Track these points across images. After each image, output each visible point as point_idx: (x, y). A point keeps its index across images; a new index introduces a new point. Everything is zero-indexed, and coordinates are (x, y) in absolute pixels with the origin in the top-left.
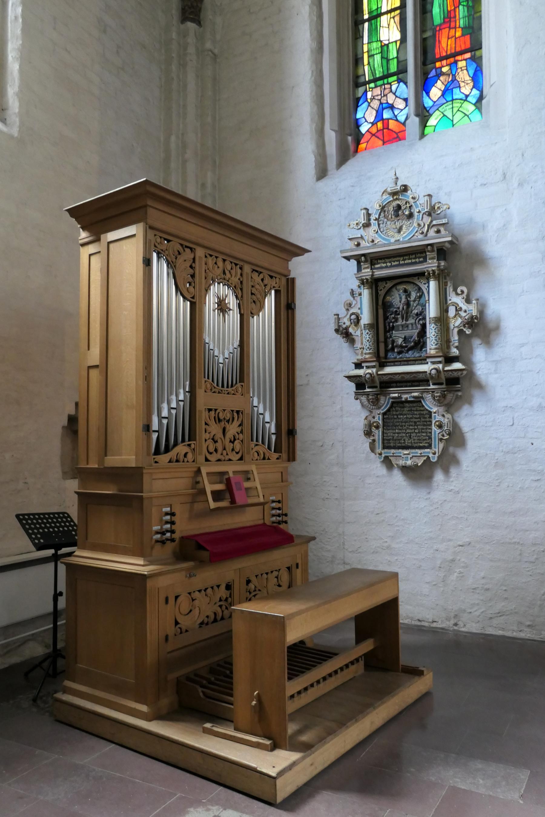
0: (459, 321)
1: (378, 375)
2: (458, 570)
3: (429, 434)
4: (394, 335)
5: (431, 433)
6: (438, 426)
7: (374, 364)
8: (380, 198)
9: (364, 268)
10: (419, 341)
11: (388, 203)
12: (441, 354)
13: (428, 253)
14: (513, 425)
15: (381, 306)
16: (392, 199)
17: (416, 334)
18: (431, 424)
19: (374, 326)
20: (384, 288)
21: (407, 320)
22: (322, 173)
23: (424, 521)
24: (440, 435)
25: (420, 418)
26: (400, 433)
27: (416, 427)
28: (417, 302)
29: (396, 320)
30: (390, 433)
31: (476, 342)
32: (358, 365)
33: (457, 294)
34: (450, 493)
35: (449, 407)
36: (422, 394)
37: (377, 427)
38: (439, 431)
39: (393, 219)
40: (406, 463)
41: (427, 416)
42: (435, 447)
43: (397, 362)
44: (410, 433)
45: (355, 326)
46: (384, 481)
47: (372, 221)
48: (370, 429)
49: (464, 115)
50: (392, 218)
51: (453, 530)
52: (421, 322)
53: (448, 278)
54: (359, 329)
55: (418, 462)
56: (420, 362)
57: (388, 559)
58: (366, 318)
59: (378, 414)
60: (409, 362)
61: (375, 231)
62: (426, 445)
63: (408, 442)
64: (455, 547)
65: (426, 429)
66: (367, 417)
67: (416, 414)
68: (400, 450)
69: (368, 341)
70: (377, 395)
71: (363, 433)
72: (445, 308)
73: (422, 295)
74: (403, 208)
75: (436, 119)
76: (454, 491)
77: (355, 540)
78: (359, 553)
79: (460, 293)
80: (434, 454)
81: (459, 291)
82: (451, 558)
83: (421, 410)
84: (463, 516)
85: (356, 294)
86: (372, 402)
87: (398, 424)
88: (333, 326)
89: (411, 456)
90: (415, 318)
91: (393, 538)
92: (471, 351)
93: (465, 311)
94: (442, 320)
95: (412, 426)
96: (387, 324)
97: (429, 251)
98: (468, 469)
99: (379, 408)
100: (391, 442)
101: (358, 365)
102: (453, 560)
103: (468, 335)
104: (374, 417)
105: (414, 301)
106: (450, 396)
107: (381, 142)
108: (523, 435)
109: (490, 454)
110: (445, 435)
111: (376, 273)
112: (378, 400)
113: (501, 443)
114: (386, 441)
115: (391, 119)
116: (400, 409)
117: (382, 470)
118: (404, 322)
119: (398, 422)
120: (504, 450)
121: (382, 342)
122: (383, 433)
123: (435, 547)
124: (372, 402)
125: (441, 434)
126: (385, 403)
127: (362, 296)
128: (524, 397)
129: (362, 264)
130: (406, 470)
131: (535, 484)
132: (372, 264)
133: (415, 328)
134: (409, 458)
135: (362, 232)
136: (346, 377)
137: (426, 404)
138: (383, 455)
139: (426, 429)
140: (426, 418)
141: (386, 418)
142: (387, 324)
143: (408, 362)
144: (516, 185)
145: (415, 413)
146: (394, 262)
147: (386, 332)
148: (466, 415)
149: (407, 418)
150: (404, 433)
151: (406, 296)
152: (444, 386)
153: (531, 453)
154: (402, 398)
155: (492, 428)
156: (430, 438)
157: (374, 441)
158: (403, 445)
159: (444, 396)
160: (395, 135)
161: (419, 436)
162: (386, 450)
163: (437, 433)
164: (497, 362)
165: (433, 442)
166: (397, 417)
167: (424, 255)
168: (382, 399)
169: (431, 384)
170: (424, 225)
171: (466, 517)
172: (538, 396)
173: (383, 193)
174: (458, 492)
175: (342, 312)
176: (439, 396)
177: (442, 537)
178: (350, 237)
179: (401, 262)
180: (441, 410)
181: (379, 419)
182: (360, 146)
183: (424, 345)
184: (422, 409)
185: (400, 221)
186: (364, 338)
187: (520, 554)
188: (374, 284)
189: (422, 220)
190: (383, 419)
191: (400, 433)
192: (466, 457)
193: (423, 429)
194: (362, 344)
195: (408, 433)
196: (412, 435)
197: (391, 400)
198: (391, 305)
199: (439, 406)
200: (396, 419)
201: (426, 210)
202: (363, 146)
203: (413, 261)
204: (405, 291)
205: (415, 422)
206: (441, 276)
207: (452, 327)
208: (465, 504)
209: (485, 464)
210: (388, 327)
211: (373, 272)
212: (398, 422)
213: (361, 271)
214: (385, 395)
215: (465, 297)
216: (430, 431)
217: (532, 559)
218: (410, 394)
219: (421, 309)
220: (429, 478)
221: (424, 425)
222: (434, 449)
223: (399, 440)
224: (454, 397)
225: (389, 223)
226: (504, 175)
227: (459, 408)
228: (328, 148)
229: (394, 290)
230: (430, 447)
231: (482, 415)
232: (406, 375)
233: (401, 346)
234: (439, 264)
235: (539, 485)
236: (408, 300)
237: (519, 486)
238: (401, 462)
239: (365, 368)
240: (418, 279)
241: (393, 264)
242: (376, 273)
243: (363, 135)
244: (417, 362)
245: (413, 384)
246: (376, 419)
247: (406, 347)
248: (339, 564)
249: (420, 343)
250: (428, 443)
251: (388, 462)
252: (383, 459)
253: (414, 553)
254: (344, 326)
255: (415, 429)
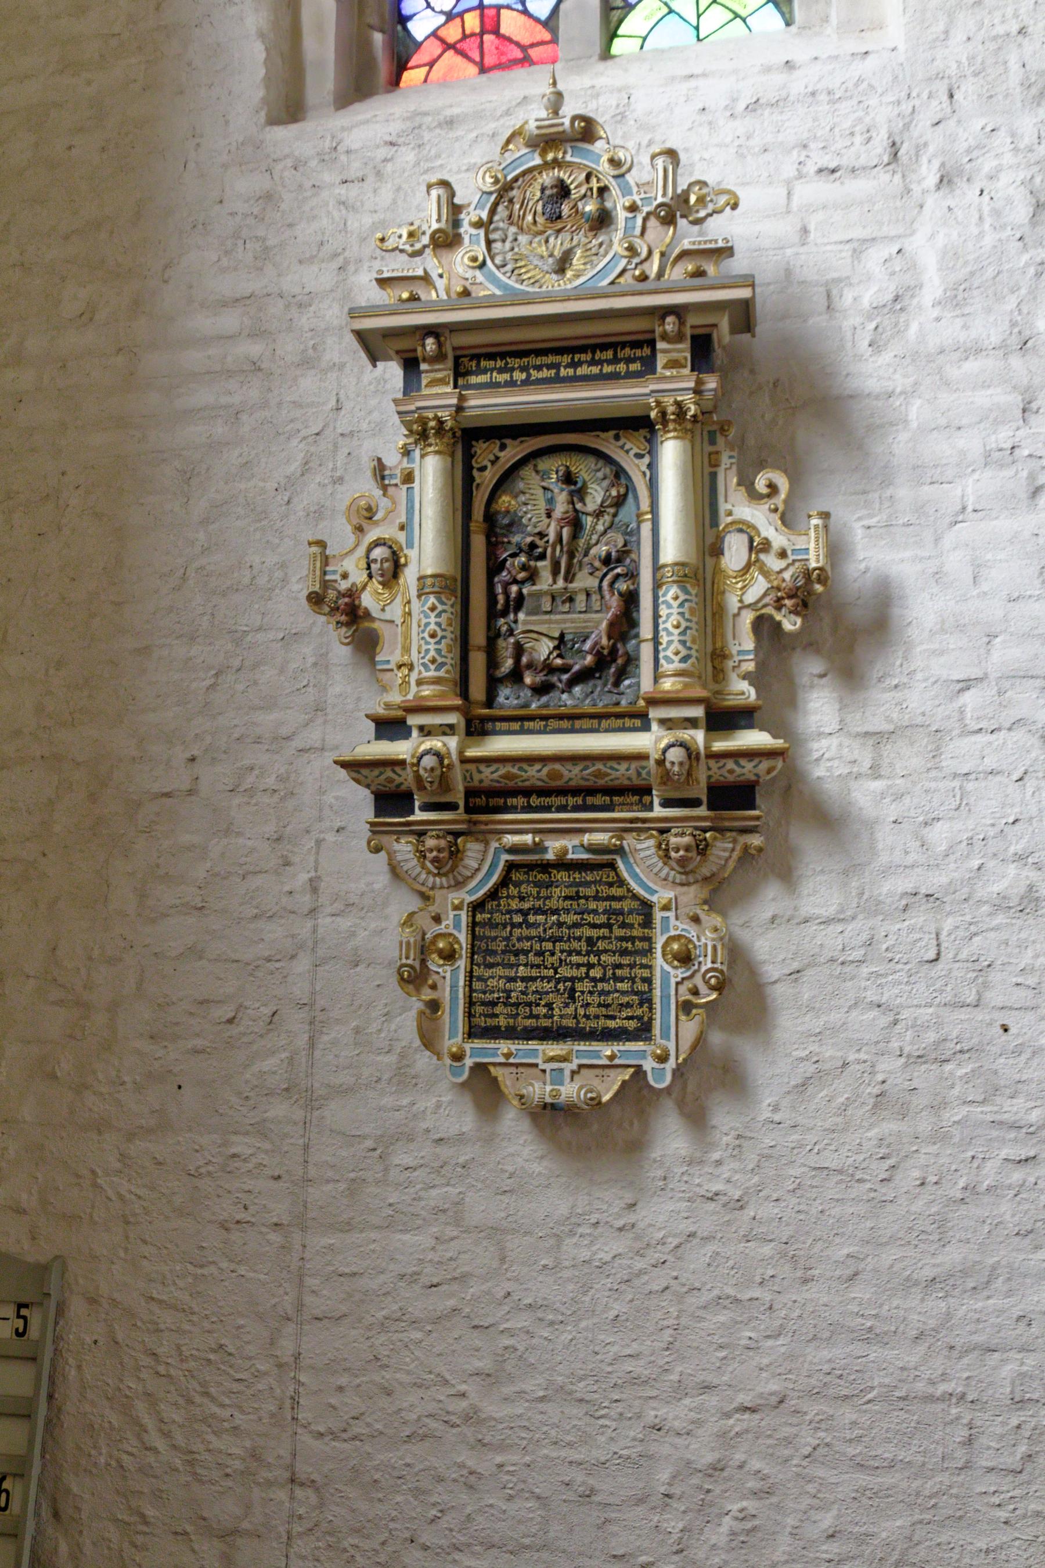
0: (758, 588)
1: (464, 760)
2: (735, 1507)
3: (641, 987)
4: (520, 628)
5: (648, 981)
6: (676, 957)
7: (452, 718)
8: (497, 157)
9: (432, 383)
10: (614, 651)
11: (524, 173)
12: (699, 692)
13: (660, 345)
14: (936, 960)
15: (481, 524)
16: (537, 161)
17: (604, 625)
18: (650, 950)
19: (455, 587)
20: (493, 463)
21: (569, 577)
22: (289, 107)
23: (612, 1314)
24: (683, 989)
25: (609, 926)
26: (533, 979)
27: (593, 959)
28: (607, 518)
29: (533, 576)
30: (496, 980)
31: (809, 667)
32: (389, 726)
33: (754, 496)
34: (711, 1206)
35: (719, 892)
36: (621, 839)
37: (449, 956)
38: (681, 973)
39: (540, 227)
40: (556, 1094)
41: (636, 919)
42: (665, 1036)
43: (531, 718)
44: (572, 979)
45: (384, 584)
46: (462, 1160)
47: (466, 229)
48: (423, 962)
49: (732, 16)
50: (535, 222)
51: (721, 1347)
52: (623, 586)
53: (720, 440)
54: (399, 600)
55: (600, 1088)
56: (619, 722)
57: (470, 1463)
58: (428, 553)
59: (457, 908)
60: (578, 724)
61: (474, 259)
62: (632, 1025)
63: (563, 1014)
64: (728, 1415)
65: (632, 966)
66: (412, 915)
67: (595, 912)
68: (533, 1045)
69: (433, 636)
70: (457, 834)
71: (394, 979)
72: (710, 540)
73: (626, 495)
74: (575, 194)
75: (647, 18)
76: (723, 1199)
77: (340, 1389)
78: (354, 1438)
79: (764, 490)
80: (663, 1059)
81: (761, 484)
82: (709, 1458)
83: (613, 898)
84: (756, 1293)
85: (391, 476)
86: (434, 861)
87: (527, 945)
88: (300, 586)
89: (574, 1066)
90: (599, 574)
91: (489, 1378)
92: (791, 700)
93: (783, 554)
94: (702, 576)
95: (579, 953)
96: (499, 589)
97: (665, 337)
98: (777, 1118)
99: (459, 885)
100: (498, 1010)
101: (389, 726)
102: (717, 1468)
103: (790, 634)
104: (437, 919)
105: (598, 514)
106: (723, 849)
107: (472, 70)
108: (971, 998)
109: (859, 1062)
110: (703, 989)
111: (472, 403)
112: (455, 854)
113: (895, 1022)
114: (479, 1009)
115: (508, 7)
116: (534, 891)
117: (458, 1117)
118: (561, 583)
119: (529, 938)
120: (907, 1049)
121: (479, 648)
122: (470, 976)
123: (650, 1416)
124: (434, 861)
125: (688, 984)
126: (483, 865)
127: (416, 485)
128: (976, 863)
129: (424, 366)
130: (550, 1116)
131: (1017, 1176)
132: (459, 373)
133: (597, 606)
134: (567, 1073)
135: (430, 263)
136: (344, 765)
137: (635, 876)
138: (469, 1062)
139: (632, 966)
140: (631, 926)
141: (483, 924)
142: (499, 589)
143: (572, 721)
144: (932, 180)
145: (592, 905)
146: (539, 368)
147: (493, 614)
148: (773, 919)
149: (560, 925)
150: (549, 979)
151: (571, 494)
152: (702, 811)
153: (1002, 1060)
154: (545, 850)
155: (865, 970)
156: (646, 1000)
157: (434, 1006)
158: (545, 1023)
159: (702, 849)
160: (518, 54)
161: (603, 993)
162: (478, 1044)
163: (673, 981)
164: (878, 738)
165: (658, 1016)
166: (525, 921)
167: (647, 351)
168: (472, 849)
169: (656, 801)
170: (650, 253)
171: (767, 1297)
172: (1020, 858)
173: (508, 142)
174: (740, 1205)
175: (340, 534)
176: (687, 849)
177: (674, 1377)
178: (386, 275)
179: (563, 372)
180: (691, 895)
181: (457, 925)
182: (406, 75)
183: (629, 666)
184: (615, 891)
185: (565, 236)
186: (415, 630)
187: (969, 1441)
188: (466, 439)
189: (643, 233)
190: (473, 925)
191: (533, 979)
192: (773, 1069)
193: (619, 966)
194: (407, 650)
195: (566, 979)
196: (579, 986)
197: (505, 857)
198: (516, 524)
199: (682, 885)
200: (520, 925)
201: (660, 200)
202: (412, 76)
203: (608, 369)
204: (568, 479)
205: (590, 941)
206: (706, 430)
207: (733, 602)
208: (767, 1250)
209: (841, 1100)
210: (501, 599)
211: (462, 398)
212: (529, 938)
213: (419, 389)
214: (483, 836)
215: (781, 508)
216: (646, 973)
217: (1012, 1460)
218: (571, 838)
219: (620, 543)
220: (635, 1147)
221: (624, 952)
222: (660, 1041)
223: (529, 1004)
224: (736, 855)
225: (523, 239)
226: (894, 148)
227: (748, 894)
228: (310, 44)
229: (527, 472)
230: (643, 1031)
231: (827, 922)
232: (569, 765)
233: (549, 669)
234: (699, 382)
235: (1032, 1180)
236: (576, 510)
237: (961, 1184)
238: (539, 1090)
239: (415, 733)
240: (617, 438)
241: (535, 374)
242: (472, 403)
243: (418, 45)
244: (605, 723)
245: (590, 800)
246: (447, 924)
247: (565, 669)
248: (269, 1484)
249: (613, 662)
250: (640, 1018)
251: (484, 1087)
252: (466, 1075)
253: (569, 1438)
254: (344, 585)
255: (590, 966)
